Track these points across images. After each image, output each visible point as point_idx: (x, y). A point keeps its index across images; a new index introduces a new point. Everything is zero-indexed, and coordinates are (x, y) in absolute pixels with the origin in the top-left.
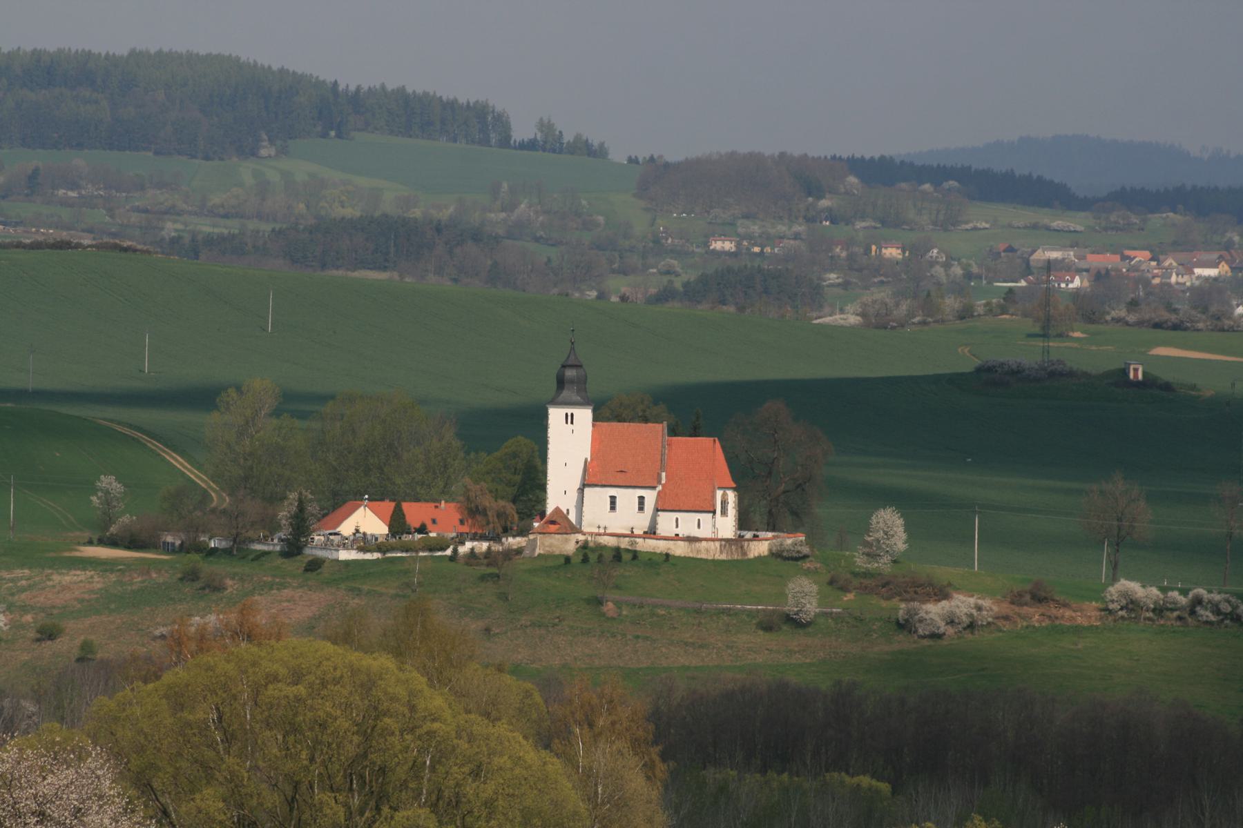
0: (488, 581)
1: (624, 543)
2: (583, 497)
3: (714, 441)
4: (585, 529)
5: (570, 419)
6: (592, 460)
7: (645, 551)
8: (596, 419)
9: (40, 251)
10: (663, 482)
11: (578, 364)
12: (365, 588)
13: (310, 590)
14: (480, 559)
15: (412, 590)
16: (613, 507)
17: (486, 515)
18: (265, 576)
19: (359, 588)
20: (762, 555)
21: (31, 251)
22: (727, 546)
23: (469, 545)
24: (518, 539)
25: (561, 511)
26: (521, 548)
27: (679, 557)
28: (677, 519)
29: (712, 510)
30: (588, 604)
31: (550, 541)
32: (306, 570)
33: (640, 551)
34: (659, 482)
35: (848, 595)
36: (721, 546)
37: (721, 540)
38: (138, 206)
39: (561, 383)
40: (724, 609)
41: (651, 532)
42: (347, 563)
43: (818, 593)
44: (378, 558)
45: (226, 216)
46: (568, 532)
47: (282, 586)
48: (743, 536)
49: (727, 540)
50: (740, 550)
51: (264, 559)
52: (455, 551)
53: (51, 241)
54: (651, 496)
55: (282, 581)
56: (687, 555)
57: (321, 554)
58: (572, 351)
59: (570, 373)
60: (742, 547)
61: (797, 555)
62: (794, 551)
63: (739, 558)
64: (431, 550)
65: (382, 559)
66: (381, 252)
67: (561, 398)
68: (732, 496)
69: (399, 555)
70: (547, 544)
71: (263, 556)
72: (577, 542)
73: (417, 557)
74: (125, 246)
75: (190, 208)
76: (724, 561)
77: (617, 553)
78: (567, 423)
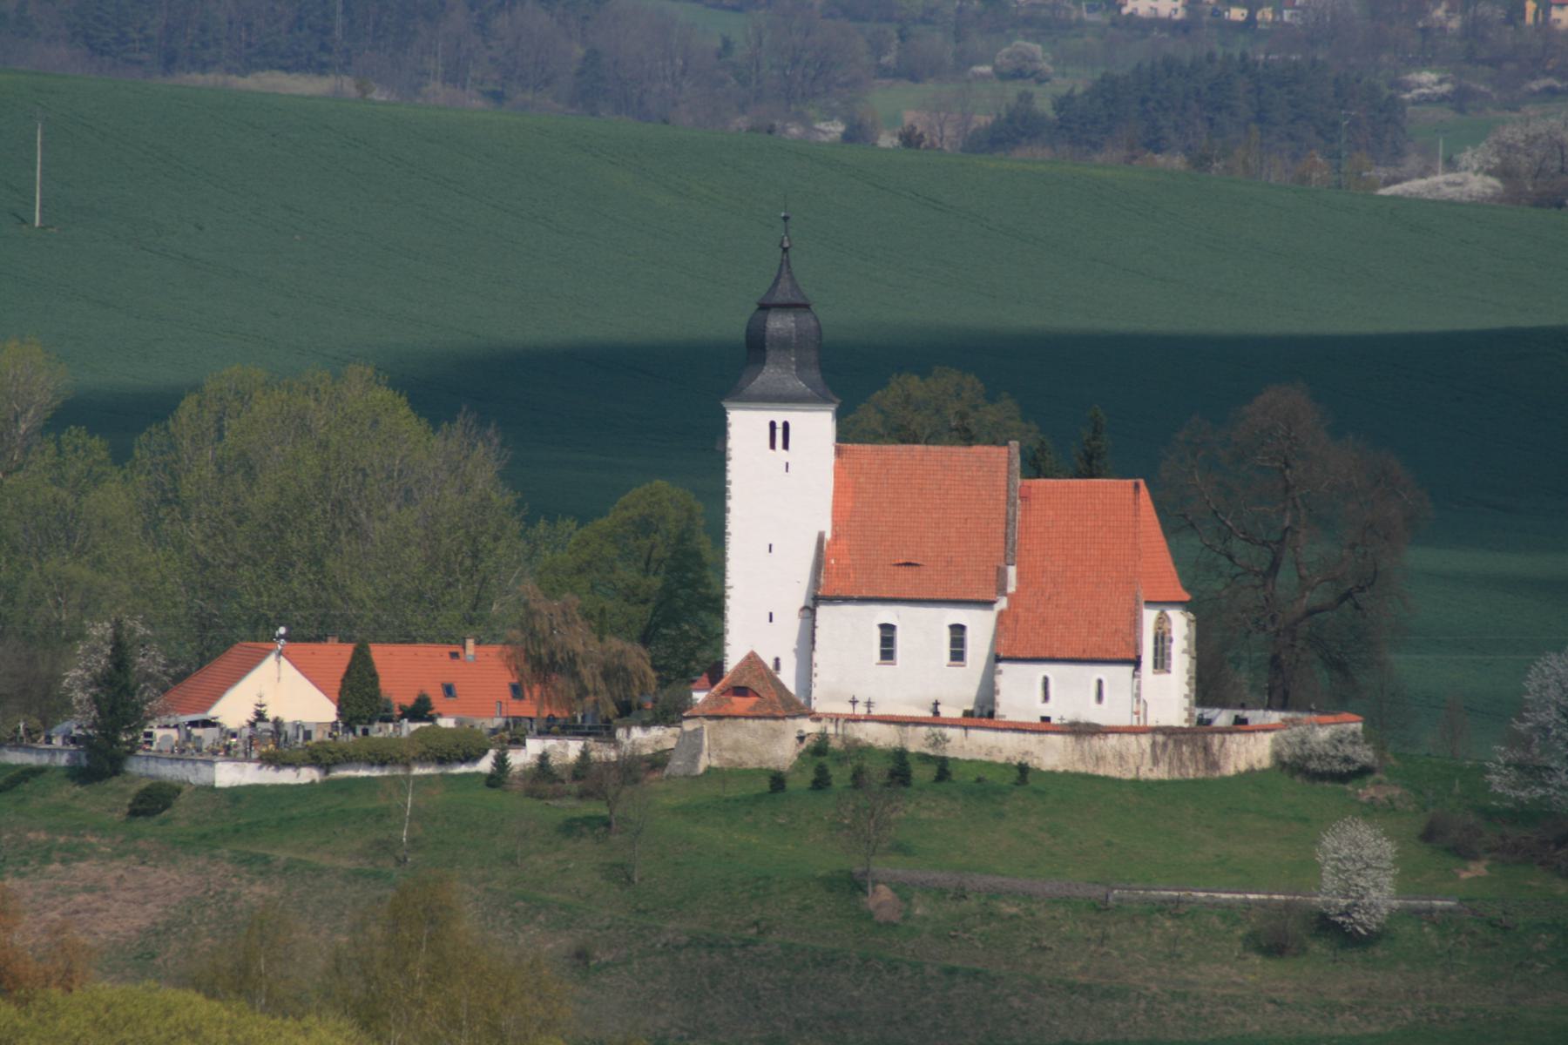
0: (582, 835)
1: (917, 740)
2: (814, 627)
3: (1137, 486)
4: (819, 706)
5: (780, 436)
6: (836, 536)
7: (967, 758)
8: (844, 435)
10: (1011, 589)
11: (801, 301)
12: (281, 855)
13: (143, 863)
14: (563, 781)
16: (888, 653)
17: (575, 675)
18: (30, 830)
19: (265, 857)
20: (1257, 766)
23: (534, 747)
27: (1052, 774)
28: (1046, 681)
29: (1132, 656)
30: (831, 891)
31: (735, 735)
33: (956, 759)
34: (1002, 590)
36: (1154, 744)
41: (983, 713)
42: (236, 795)
44: (313, 782)
46: (778, 714)
47: (73, 854)
49: (1169, 732)
50: (1200, 756)
51: (26, 786)
52: (501, 762)
54: (980, 625)
55: (75, 840)
56: (1071, 769)
59: (779, 324)
60: (1207, 749)
61: (1344, 768)
62: (1333, 757)
63: (1201, 775)
64: (441, 761)
65: (322, 782)
68: (1179, 623)
70: (726, 742)
71: (27, 780)
72: (801, 739)
73: (407, 778)
76: (1160, 783)
77: (900, 765)
78: (773, 446)
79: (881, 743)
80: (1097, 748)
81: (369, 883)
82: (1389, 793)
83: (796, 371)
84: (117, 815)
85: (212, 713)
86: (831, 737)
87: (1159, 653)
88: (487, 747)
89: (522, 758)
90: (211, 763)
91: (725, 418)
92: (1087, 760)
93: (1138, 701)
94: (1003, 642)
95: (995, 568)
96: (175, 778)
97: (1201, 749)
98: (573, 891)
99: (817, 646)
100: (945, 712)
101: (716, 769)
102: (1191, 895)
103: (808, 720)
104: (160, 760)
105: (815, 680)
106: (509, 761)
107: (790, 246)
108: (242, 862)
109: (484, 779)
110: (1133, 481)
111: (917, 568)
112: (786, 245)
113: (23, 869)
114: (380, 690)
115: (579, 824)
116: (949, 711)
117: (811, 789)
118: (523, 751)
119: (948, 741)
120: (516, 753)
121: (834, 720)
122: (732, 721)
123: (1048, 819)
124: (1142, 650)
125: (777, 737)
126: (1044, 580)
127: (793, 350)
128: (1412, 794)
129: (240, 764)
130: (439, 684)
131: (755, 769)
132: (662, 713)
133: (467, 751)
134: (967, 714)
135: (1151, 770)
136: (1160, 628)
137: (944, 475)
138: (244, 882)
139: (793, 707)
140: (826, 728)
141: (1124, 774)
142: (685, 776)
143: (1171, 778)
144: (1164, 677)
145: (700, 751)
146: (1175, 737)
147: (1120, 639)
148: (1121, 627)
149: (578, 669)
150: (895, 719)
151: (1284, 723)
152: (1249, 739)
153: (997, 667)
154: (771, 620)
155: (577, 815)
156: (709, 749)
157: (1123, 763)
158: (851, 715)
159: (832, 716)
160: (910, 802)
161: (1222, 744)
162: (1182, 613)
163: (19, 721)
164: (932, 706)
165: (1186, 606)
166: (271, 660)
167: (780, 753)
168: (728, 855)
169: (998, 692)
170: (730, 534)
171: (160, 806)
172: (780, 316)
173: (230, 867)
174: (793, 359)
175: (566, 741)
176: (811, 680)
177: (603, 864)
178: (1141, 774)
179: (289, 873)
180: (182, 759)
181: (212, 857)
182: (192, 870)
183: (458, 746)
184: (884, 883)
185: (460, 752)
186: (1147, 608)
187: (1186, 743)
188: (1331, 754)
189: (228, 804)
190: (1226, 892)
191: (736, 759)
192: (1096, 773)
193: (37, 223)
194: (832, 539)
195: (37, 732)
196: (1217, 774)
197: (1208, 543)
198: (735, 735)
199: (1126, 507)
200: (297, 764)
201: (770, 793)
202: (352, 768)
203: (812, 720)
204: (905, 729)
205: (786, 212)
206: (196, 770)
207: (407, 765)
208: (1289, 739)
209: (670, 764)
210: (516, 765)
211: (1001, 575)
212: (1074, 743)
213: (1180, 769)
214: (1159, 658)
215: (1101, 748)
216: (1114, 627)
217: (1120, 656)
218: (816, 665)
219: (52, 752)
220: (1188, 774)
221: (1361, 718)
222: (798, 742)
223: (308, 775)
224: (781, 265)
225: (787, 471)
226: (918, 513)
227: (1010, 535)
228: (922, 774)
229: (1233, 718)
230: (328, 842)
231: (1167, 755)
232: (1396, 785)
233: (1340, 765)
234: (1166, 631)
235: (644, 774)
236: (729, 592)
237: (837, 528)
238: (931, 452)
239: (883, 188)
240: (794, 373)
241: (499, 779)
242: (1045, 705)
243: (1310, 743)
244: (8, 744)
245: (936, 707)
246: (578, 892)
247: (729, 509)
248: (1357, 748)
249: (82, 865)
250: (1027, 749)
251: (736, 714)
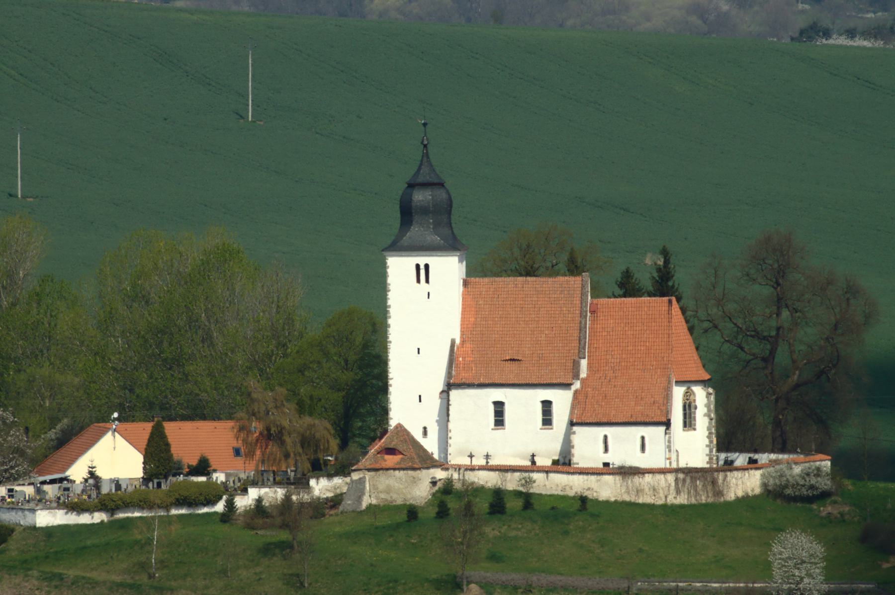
0: (274, 555)
1: (512, 482)
2: (448, 405)
3: (670, 302)
4: (456, 459)
5: (423, 273)
6: (463, 342)
8: (474, 271)
10: (583, 375)
11: (436, 181)
12: (72, 573)
14: (273, 517)
15: (149, 574)
16: (499, 421)
17: (282, 443)
19: (60, 574)
20: (750, 494)
22: (688, 480)
23: (254, 493)
24: (337, 481)
26: (342, 494)
27: (607, 502)
28: (606, 437)
29: (664, 419)
31: (387, 482)
33: (540, 495)
34: (576, 376)
36: (677, 480)
37: (678, 470)
39: (407, 213)
42: (49, 532)
43: (824, 559)
44: (102, 522)
46: (416, 466)
48: (732, 462)
49: (689, 472)
50: (709, 488)
52: (230, 505)
54: (562, 400)
56: (619, 499)
58: (425, 159)
59: (420, 197)
60: (714, 482)
61: (810, 493)
62: (803, 486)
63: (710, 500)
65: (109, 522)
68: (701, 395)
69: (137, 514)
70: (381, 487)
72: (434, 483)
73: (168, 516)
76: (682, 506)
77: (498, 497)
78: (418, 281)
79: (490, 485)
82: (841, 510)
83: (433, 229)
85: (68, 473)
86: (455, 481)
89: (244, 502)
90: (33, 511)
91: (385, 263)
93: (670, 451)
95: (572, 361)
96: (11, 522)
97: (710, 483)
99: (451, 418)
100: (540, 462)
101: (375, 506)
102: (690, 585)
105: (450, 441)
106: (236, 504)
107: (428, 143)
109: (220, 516)
110: (667, 298)
111: (519, 362)
112: (426, 142)
114: (172, 455)
115: (272, 546)
116: (541, 462)
117: (436, 517)
118: (246, 497)
119: (534, 482)
120: (242, 498)
122: (385, 472)
123: (599, 534)
124: (671, 415)
126: (607, 368)
127: (431, 215)
129: (53, 511)
130: (231, 448)
131: (401, 505)
133: (208, 497)
134: (555, 463)
136: (687, 400)
137: (537, 298)
139: (428, 462)
140: (452, 475)
142: (353, 511)
143: (689, 503)
144: (692, 433)
145: (363, 494)
146: (691, 474)
147: (657, 408)
150: (499, 468)
152: (745, 475)
154: (420, 401)
157: (656, 494)
158: (469, 466)
159: (456, 467)
160: (504, 525)
164: (530, 458)
166: (109, 436)
167: (418, 493)
168: (372, 565)
169: (573, 447)
172: (421, 192)
173: (36, 583)
174: (431, 221)
175: (276, 488)
177: (285, 575)
178: (668, 501)
179: (74, 586)
181: (26, 576)
183: (201, 494)
184: (476, 583)
185: (202, 498)
187: (699, 479)
189: (44, 538)
191: (389, 499)
192: (637, 502)
193: (250, 119)
196: (722, 500)
197: (727, 339)
198: (387, 482)
201: (408, 521)
202: (130, 512)
203: (442, 469)
204: (506, 474)
205: (425, 120)
206: (24, 516)
207: (168, 511)
209: (343, 503)
212: (621, 481)
213: (696, 497)
214: (687, 420)
216: (653, 399)
218: (450, 431)
220: (701, 500)
221: (830, 458)
222: (431, 485)
223: (99, 517)
224: (423, 156)
225: (429, 298)
226: (520, 324)
228: (514, 505)
229: (747, 459)
230: (106, 564)
232: (846, 504)
234: (692, 401)
235: (328, 511)
236: (391, 382)
237: (464, 336)
238: (528, 282)
243: (786, 476)
245: (533, 458)
247: (389, 325)
248: (819, 479)
250: (589, 486)
251: (387, 467)
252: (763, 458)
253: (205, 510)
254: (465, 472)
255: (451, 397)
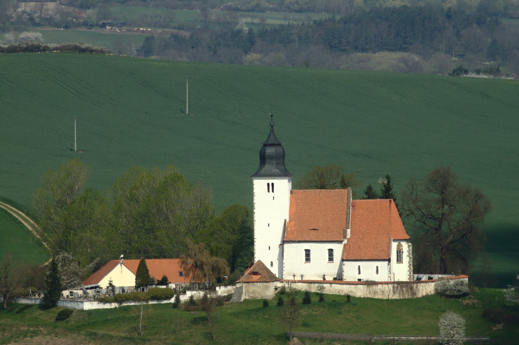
0: (199, 323)
1: (314, 288)
2: (283, 251)
3: (390, 201)
5: (271, 188)
6: (290, 221)
7: (332, 294)
9: (14, 54)
10: (348, 236)
11: (277, 143)
13: (56, 336)
14: (198, 305)
15: (138, 333)
17: (203, 269)
18: (22, 326)
19: (95, 333)
20: (429, 294)
21: (9, 54)
22: (399, 288)
23: (189, 294)
25: (263, 265)
27: (360, 298)
28: (359, 267)
29: (387, 258)
30: (278, 340)
31: (254, 288)
32: (58, 319)
33: (328, 294)
34: (345, 237)
35: (498, 325)
36: (393, 287)
37: (394, 283)
38: (231, 6)
39: (263, 159)
40: (390, 340)
41: (339, 279)
42: (90, 312)
43: (465, 325)
44: (116, 307)
45: (300, 11)
47: (36, 333)
48: (420, 279)
49: (400, 283)
50: (409, 291)
51: (26, 311)
52: (177, 299)
53: (24, 46)
54: (338, 249)
55: (36, 329)
56: (366, 296)
57: (70, 305)
58: (272, 133)
59: (269, 151)
60: (412, 288)
61: (458, 293)
62: (455, 290)
63: (410, 297)
65: (119, 307)
66: (401, 36)
67: (263, 171)
68: (405, 246)
69: (132, 304)
70: (251, 291)
71: (26, 309)
73: (148, 305)
74: (83, 47)
75: (271, 6)
77: (307, 297)
78: (269, 191)
79: (303, 290)
80: (375, 289)
81: (127, 341)
82: (473, 302)
83: (276, 166)
84: (52, 320)
85: (99, 284)
87: (399, 257)
88: (173, 294)
89: (184, 298)
90: (82, 302)
92: (371, 293)
94: (345, 254)
95: (343, 230)
97: (410, 289)
98: (194, 342)
99: (284, 257)
101: (248, 300)
103: (279, 282)
104: (67, 302)
105: (284, 269)
106: (180, 299)
108: (88, 335)
110: (389, 199)
111: (317, 230)
112: (272, 124)
113: (17, 340)
114: (149, 275)
115: (198, 319)
117: (277, 305)
118: (185, 295)
119: (325, 288)
120: (183, 296)
121: (288, 282)
122: (252, 283)
125: (267, 288)
127: (274, 159)
128: (481, 302)
129: (92, 302)
132: (231, 281)
133: (167, 296)
135: (393, 296)
136: (399, 248)
137: (326, 199)
138: (87, 342)
140: (285, 285)
141: (384, 298)
143: (400, 299)
145: (242, 294)
146: (400, 285)
147: (384, 252)
148: (384, 248)
149: (204, 267)
150: (307, 281)
151: (439, 279)
153: (343, 263)
155: (199, 316)
156: (245, 293)
157: (384, 294)
158: (293, 280)
159: (287, 281)
160: (310, 309)
161: (417, 287)
162: (406, 243)
163: (29, 289)
164: (323, 277)
165: (406, 240)
170: (255, 221)
171: (66, 317)
173: (84, 337)
174: (275, 162)
175: (200, 291)
176: (283, 269)
177: (204, 333)
178: (390, 297)
179: (102, 339)
180: (73, 301)
181: (79, 333)
182: (71, 338)
184: (297, 337)
185: (164, 296)
186: (393, 242)
188: (454, 289)
190: (412, 337)
192: (374, 298)
193: (187, 113)
194: (289, 222)
195: (36, 292)
197: (418, 219)
198: (254, 288)
199: (387, 208)
200: (110, 302)
202: (129, 303)
203: (280, 282)
205: (272, 113)
206: (78, 305)
207: (147, 302)
208: (439, 284)
209: (232, 298)
210: (183, 300)
211: (345, 232)
212: (367, 288)
213: (403, 295)
214: (399, 258)
215: (376, 289)
216: (382, 248)
217: (383, 258)
219: (35, 299)
220: (406, 297)
221: (468, 277)
222: (275, 290)
223: (114, 305)
224: (271, 131)
227: (348, 218)
228: (315, 299)
229: (428, 277)
230: (118, 328)
231: (398, 291)
233: (457, 293)
234: (401, 249)
235: (225, 302)
236: (255, 240)
237: (291, 218)
239: (470, 92)
240: (275, 167)
241: (177, 305)
242: (359, 275)
244: (22, 297)
245: (324, 277)
246: (195, 343)
249: (36, 338)
250: (351, 290)
252: (436, 277)
253: (165, 302)
254: (291, 284)
255: (284, 248)
